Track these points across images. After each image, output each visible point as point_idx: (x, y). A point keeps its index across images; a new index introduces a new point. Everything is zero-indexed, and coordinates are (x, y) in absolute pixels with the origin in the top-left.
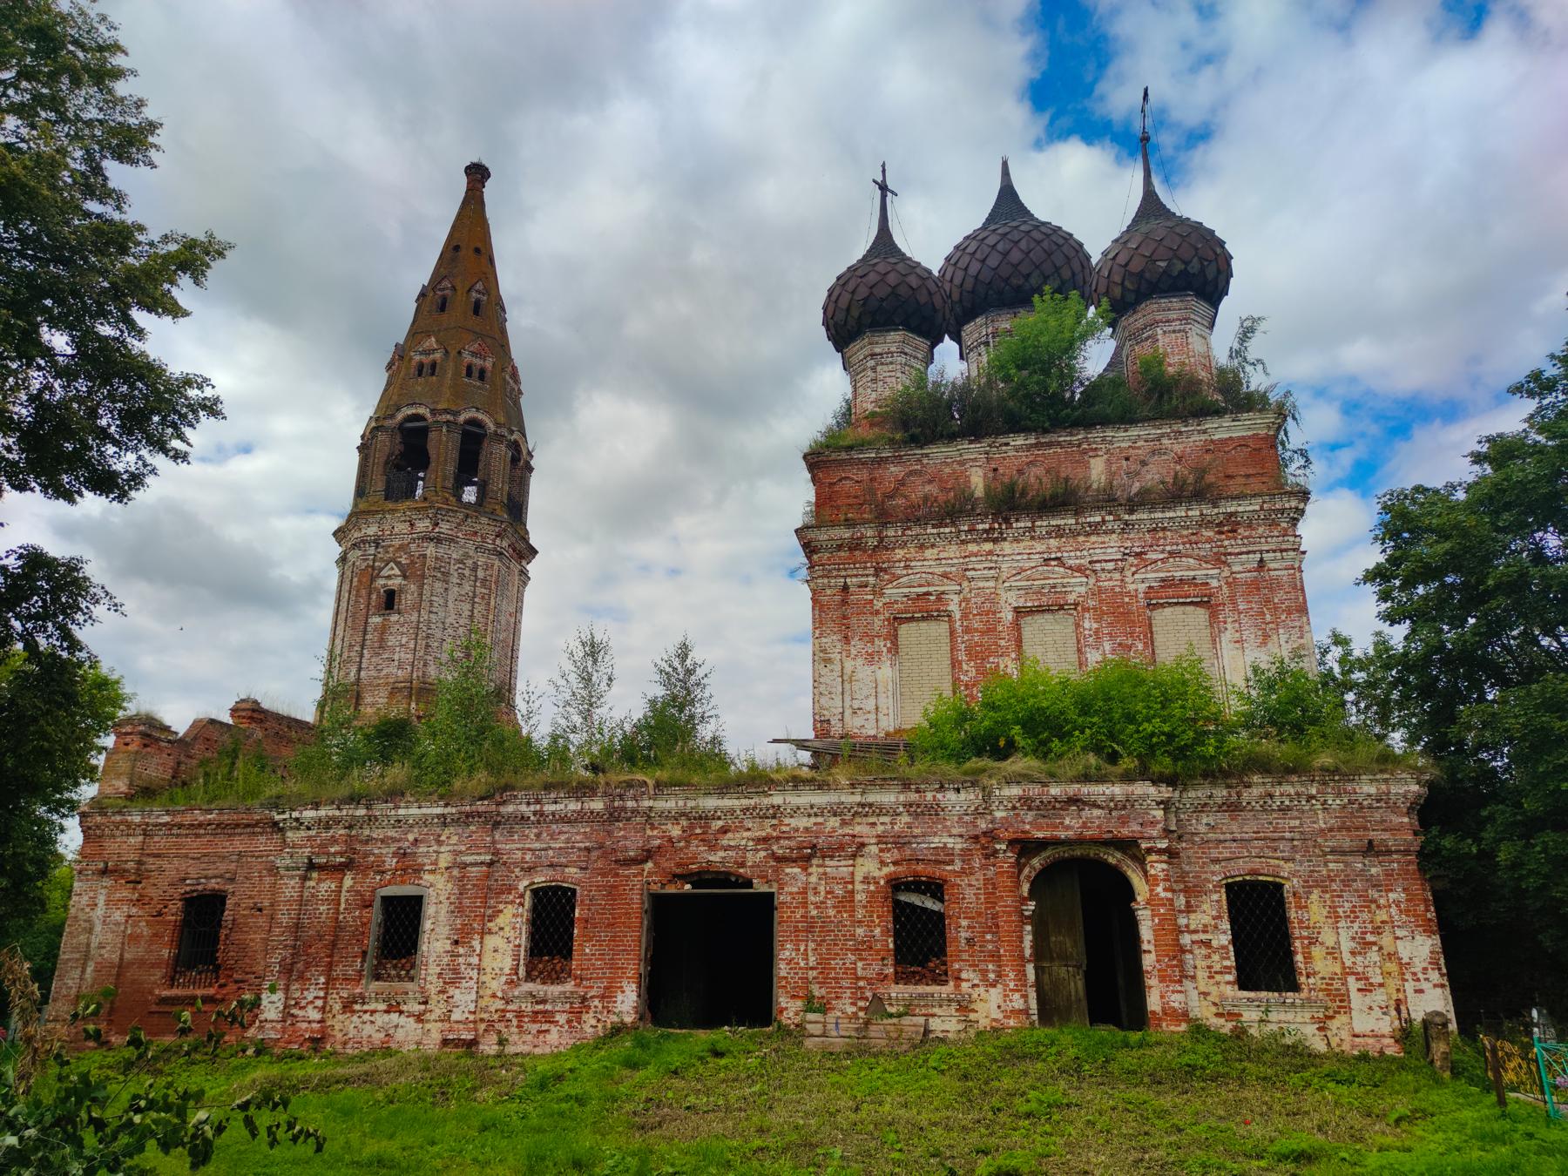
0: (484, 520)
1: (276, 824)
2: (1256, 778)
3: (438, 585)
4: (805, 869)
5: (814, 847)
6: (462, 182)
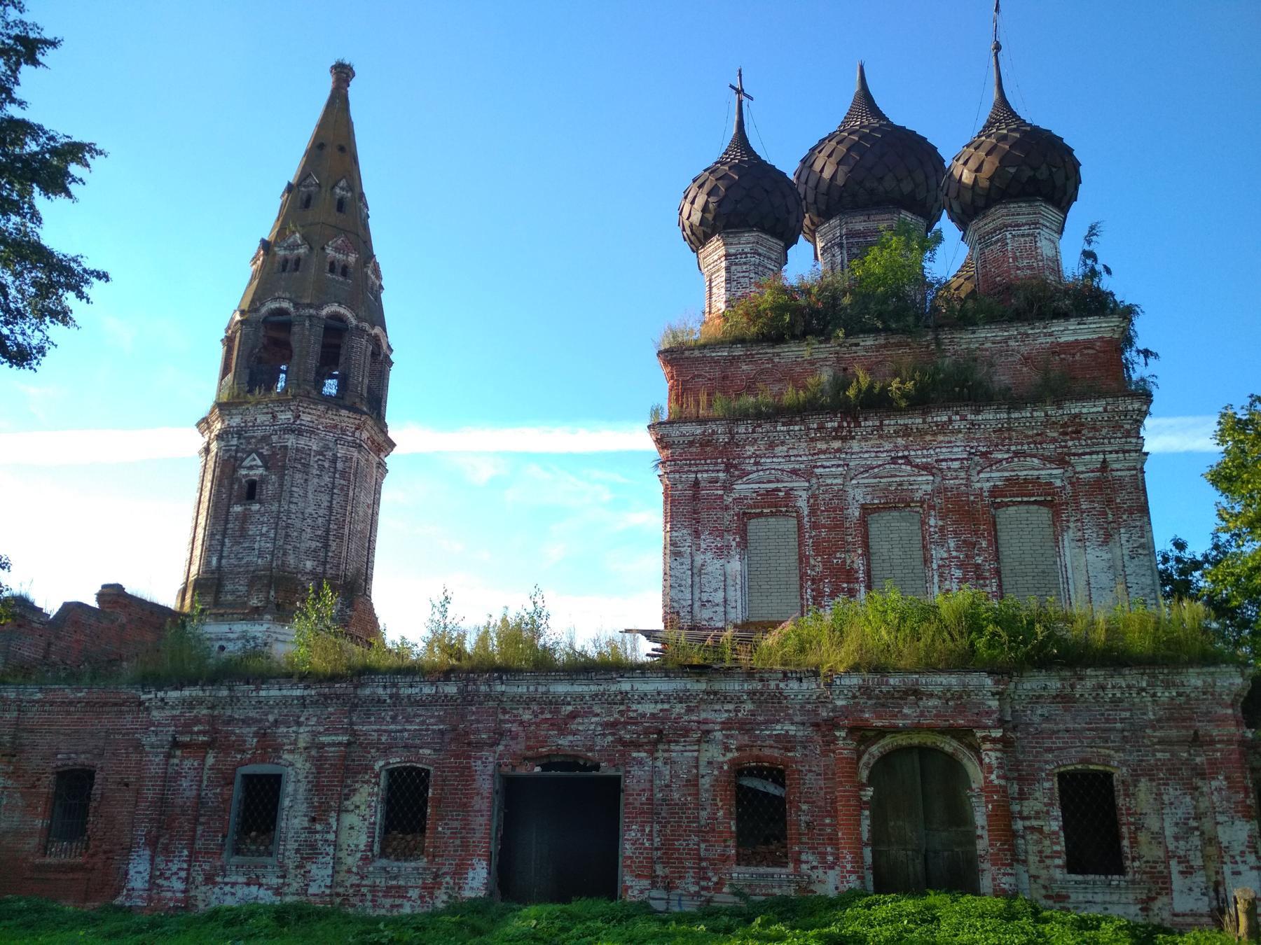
0: (344, 412)
1: (141, 703)
3: (298, 476)
5: (660, 732)
6: (326, 85)
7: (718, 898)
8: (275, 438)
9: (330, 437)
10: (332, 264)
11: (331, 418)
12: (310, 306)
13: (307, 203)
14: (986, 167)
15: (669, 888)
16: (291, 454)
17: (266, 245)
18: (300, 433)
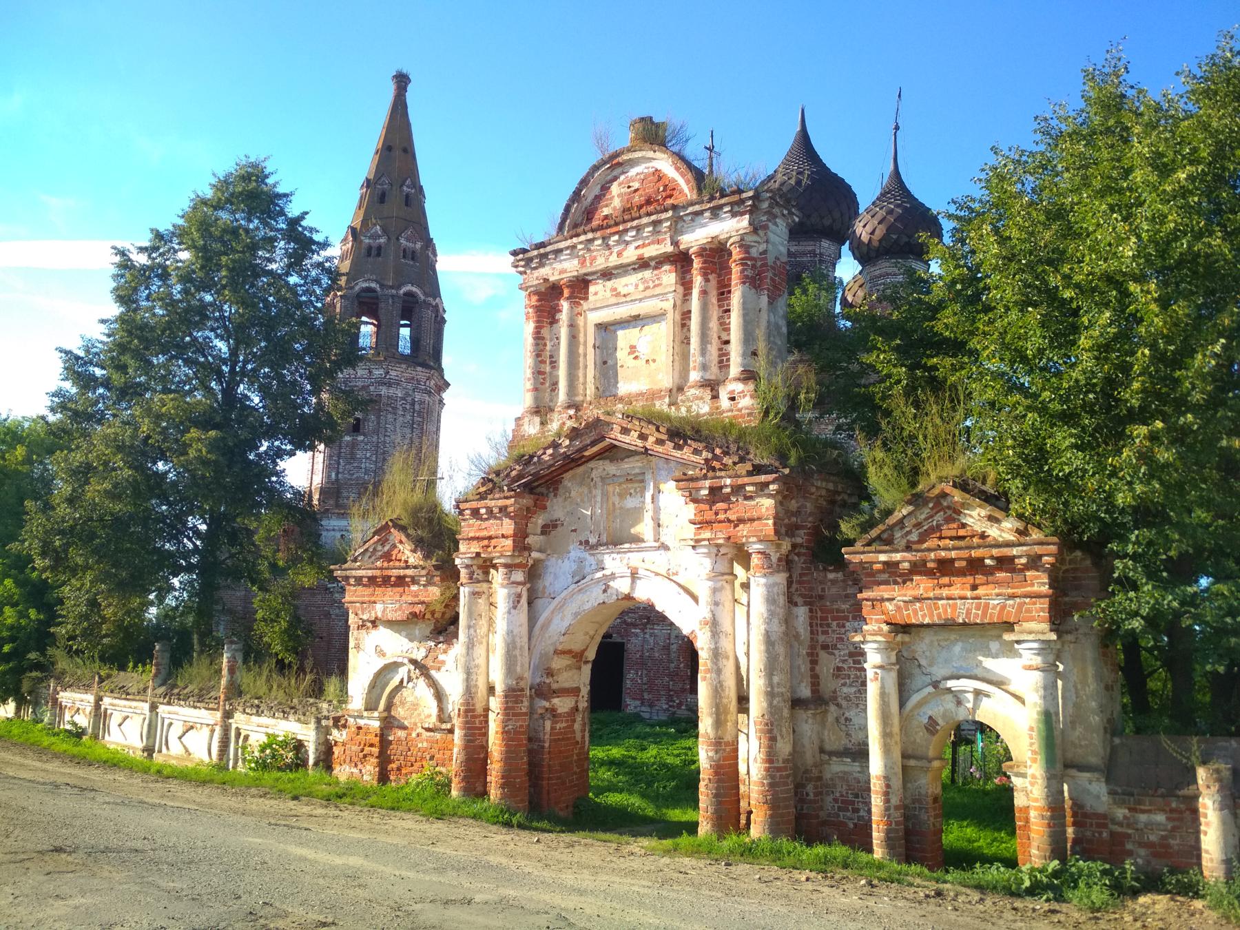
0: (419, 369)
1: (327, 589)
2: (1112, 330)
3: (390, 416)
4: (643, 630)
5: (648, 618)
6: (390, 90)
7: (679, 712)
8: (372, 388)
9: (410, 386)
10: (404, 251)
11: (410, 373)
12: (392, 287)
13: (382, 198)
14: (877, 232)
15: (651, 706)
16: (384, 400)
17: (353, 230)
18: (389, 385)
